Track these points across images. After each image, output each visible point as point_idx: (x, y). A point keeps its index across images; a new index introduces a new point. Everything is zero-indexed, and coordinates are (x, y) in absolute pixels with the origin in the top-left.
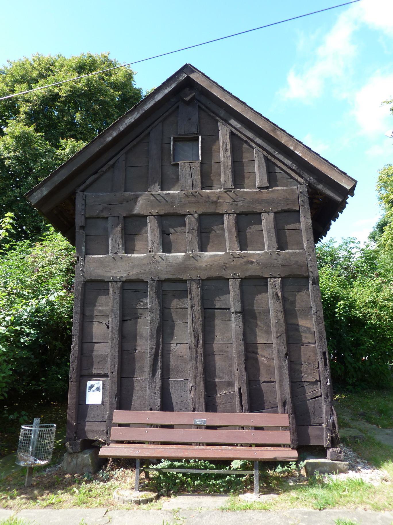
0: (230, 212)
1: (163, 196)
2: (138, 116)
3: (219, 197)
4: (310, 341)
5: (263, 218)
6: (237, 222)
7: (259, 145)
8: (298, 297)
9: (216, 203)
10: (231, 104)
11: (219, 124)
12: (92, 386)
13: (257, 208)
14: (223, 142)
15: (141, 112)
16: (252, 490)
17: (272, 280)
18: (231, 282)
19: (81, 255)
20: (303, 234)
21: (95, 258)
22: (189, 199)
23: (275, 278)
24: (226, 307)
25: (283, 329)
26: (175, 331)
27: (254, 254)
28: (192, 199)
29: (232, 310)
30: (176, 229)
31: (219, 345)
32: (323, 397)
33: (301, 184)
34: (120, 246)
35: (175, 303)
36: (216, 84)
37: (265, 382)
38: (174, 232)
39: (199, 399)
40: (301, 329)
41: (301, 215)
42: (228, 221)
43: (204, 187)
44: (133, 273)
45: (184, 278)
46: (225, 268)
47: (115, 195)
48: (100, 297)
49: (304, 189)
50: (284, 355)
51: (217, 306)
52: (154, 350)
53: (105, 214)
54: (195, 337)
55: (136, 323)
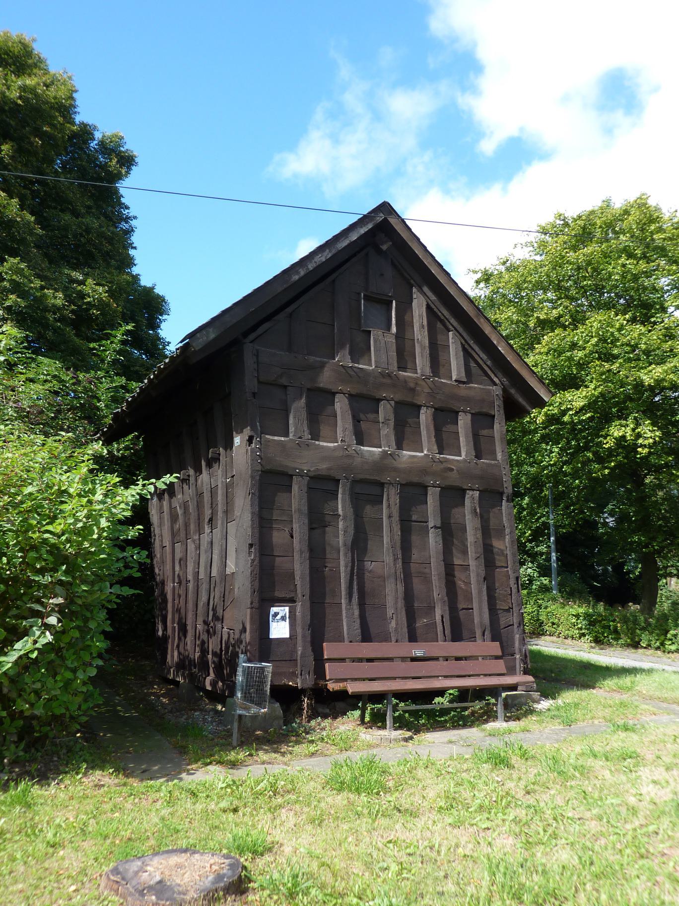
0: (428, 405)
1: (355, 369)
2: (330, 255)
3: (416, 384)
4: (503, 565)
5: (460, 418)
6: (435, 418)
7: (455, 329)
8: (491, 514)
9: (413, 390)
10: (434, 270)
11: (414, 290)
12: (276, 614)
13: (455, 405)
14: (419, 315)
15: (334, 251)
16: (495, 718)
17: (471, 493)
18: (430, 490)
19: (257, 434)
20: (461, 439)
21: (275, 440)
22: (384, 380)
23: (473, 490)
24: (423, 520)
25: (481, 550)
26: (369, 546)
27: (453, 460)
28: (387, 381)
29: (431, 524)
30: (368, 416)
31: (417, 565)
32: (515, 626)
33: (495, 384)
34: (306, 429)
35: (369, 510)
36: (418, 239)
37: (463, 609)
38: (365, 419)
39: (402, 629)
40: (495, 550)
41: (496, 421)
42: (425, 416)
43: (402, 367)
44: (323, 467)
45: (382, 481)
46: (424, 471)
47: (296, 357)
48: (279, 494)
49: (497, 391)
50: (482, 579)
51: (414, 518)
52: (349, 568)
53: (284, 381)
54: (394, 555)
55: (324, 533)
